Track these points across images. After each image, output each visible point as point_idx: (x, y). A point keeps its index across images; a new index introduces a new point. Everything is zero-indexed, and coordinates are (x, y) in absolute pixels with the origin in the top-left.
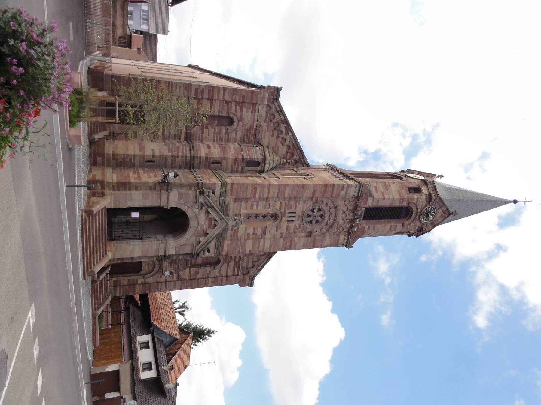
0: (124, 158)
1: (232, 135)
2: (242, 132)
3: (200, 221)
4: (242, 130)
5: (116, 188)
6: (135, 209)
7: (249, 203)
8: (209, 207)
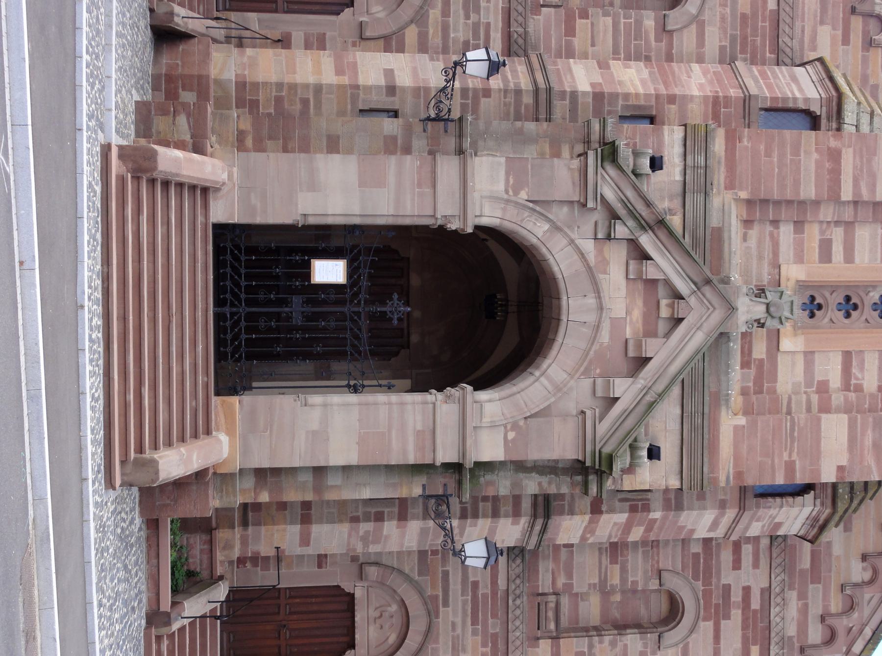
0: (279, 100)
1: (687, 40)
2: (723, 29)
3: (605, 294)
4: (723, 19)
5: (249, 142)
6: (325, 239)
7: (813, 234)
8: (644, 226)
